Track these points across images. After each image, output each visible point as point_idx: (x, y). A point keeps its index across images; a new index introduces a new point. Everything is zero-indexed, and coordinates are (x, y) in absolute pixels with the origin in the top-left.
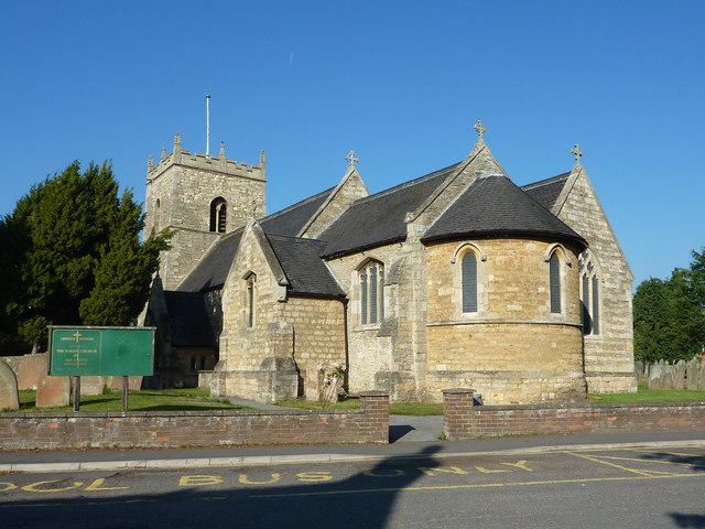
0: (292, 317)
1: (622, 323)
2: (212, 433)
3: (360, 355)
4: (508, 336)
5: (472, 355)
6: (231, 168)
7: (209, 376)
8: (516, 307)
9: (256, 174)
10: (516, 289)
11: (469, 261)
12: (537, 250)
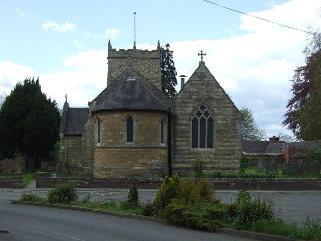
1: (232, 142)
7: (124, 200)
8: (110, 141)
10: (111, 133)
11: (130, 122)
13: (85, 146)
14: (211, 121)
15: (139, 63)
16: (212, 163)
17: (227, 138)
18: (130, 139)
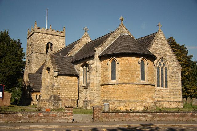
0: (60, 82)
1: (177, 84)
2: (16, 118)
3: (82, 94)
4: (125, 88)
5: (114, 94)
6: (53, 33)
9: (62, 34)
10: (129, 73)
11: (114, 63)
12: (136, 61)
13: (93, 82)
14: (166, 69)
15: (53, 38)
16: (168, 98)
17: (175, 81)
18: (143, 78)
